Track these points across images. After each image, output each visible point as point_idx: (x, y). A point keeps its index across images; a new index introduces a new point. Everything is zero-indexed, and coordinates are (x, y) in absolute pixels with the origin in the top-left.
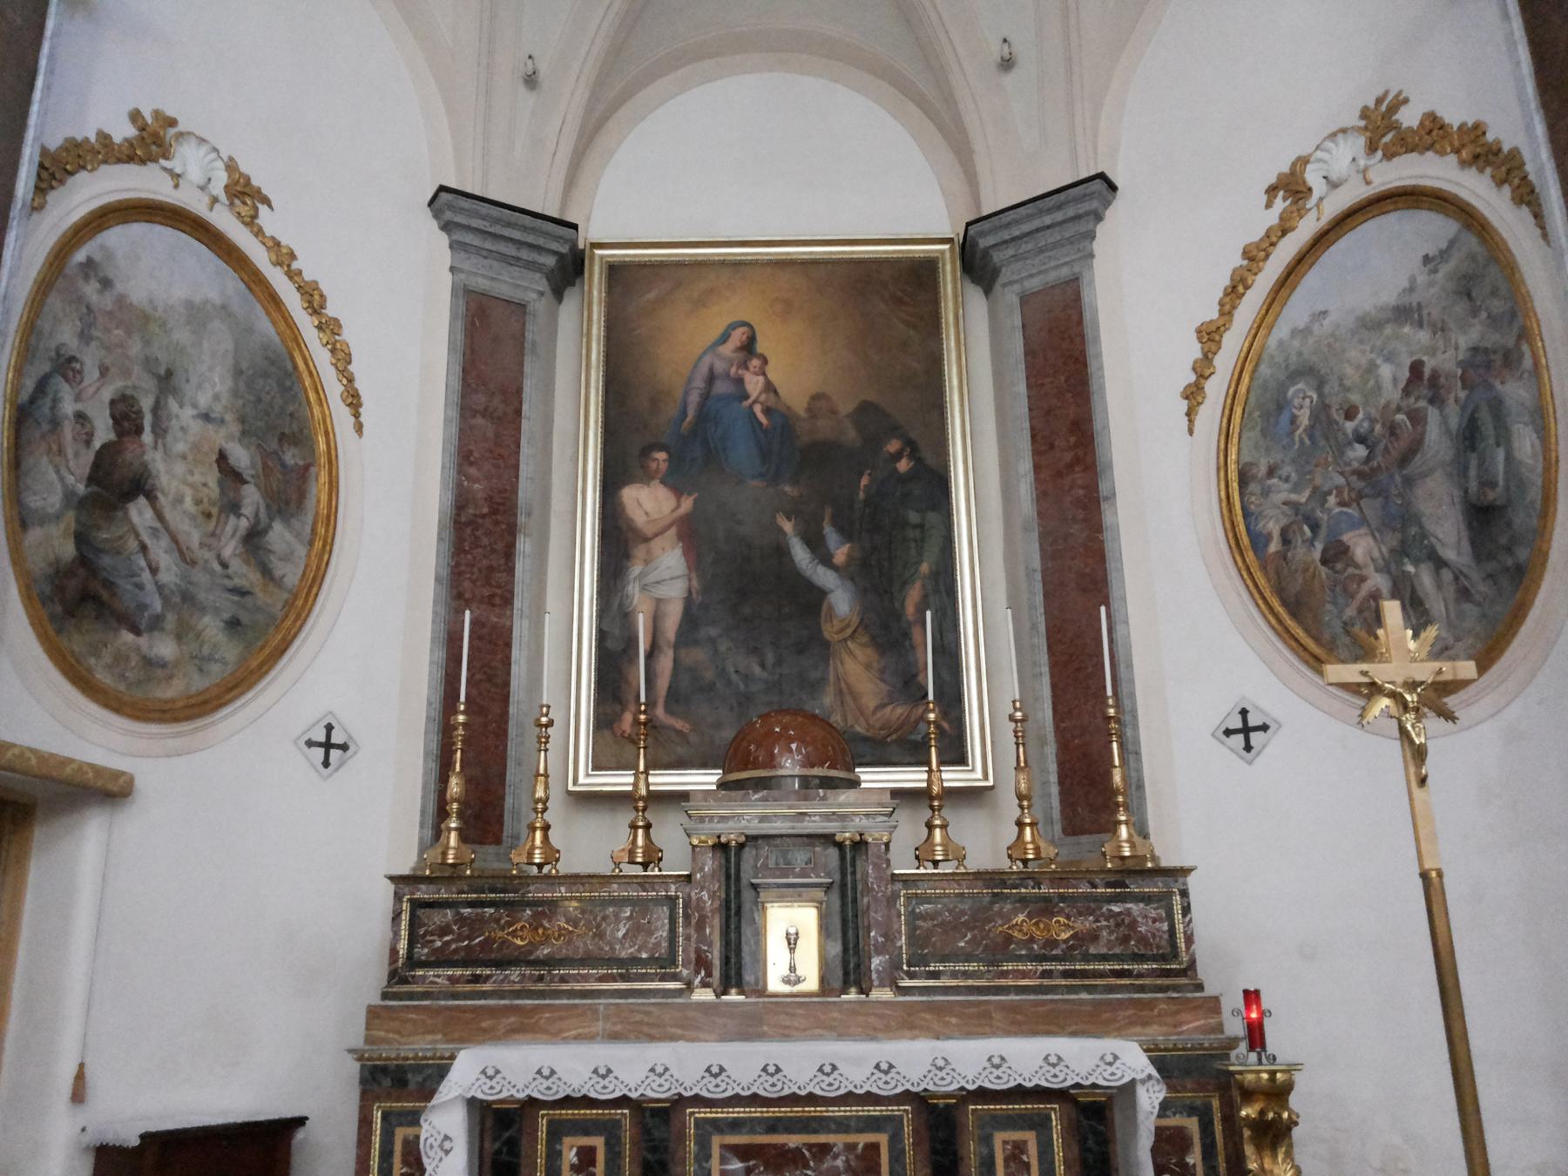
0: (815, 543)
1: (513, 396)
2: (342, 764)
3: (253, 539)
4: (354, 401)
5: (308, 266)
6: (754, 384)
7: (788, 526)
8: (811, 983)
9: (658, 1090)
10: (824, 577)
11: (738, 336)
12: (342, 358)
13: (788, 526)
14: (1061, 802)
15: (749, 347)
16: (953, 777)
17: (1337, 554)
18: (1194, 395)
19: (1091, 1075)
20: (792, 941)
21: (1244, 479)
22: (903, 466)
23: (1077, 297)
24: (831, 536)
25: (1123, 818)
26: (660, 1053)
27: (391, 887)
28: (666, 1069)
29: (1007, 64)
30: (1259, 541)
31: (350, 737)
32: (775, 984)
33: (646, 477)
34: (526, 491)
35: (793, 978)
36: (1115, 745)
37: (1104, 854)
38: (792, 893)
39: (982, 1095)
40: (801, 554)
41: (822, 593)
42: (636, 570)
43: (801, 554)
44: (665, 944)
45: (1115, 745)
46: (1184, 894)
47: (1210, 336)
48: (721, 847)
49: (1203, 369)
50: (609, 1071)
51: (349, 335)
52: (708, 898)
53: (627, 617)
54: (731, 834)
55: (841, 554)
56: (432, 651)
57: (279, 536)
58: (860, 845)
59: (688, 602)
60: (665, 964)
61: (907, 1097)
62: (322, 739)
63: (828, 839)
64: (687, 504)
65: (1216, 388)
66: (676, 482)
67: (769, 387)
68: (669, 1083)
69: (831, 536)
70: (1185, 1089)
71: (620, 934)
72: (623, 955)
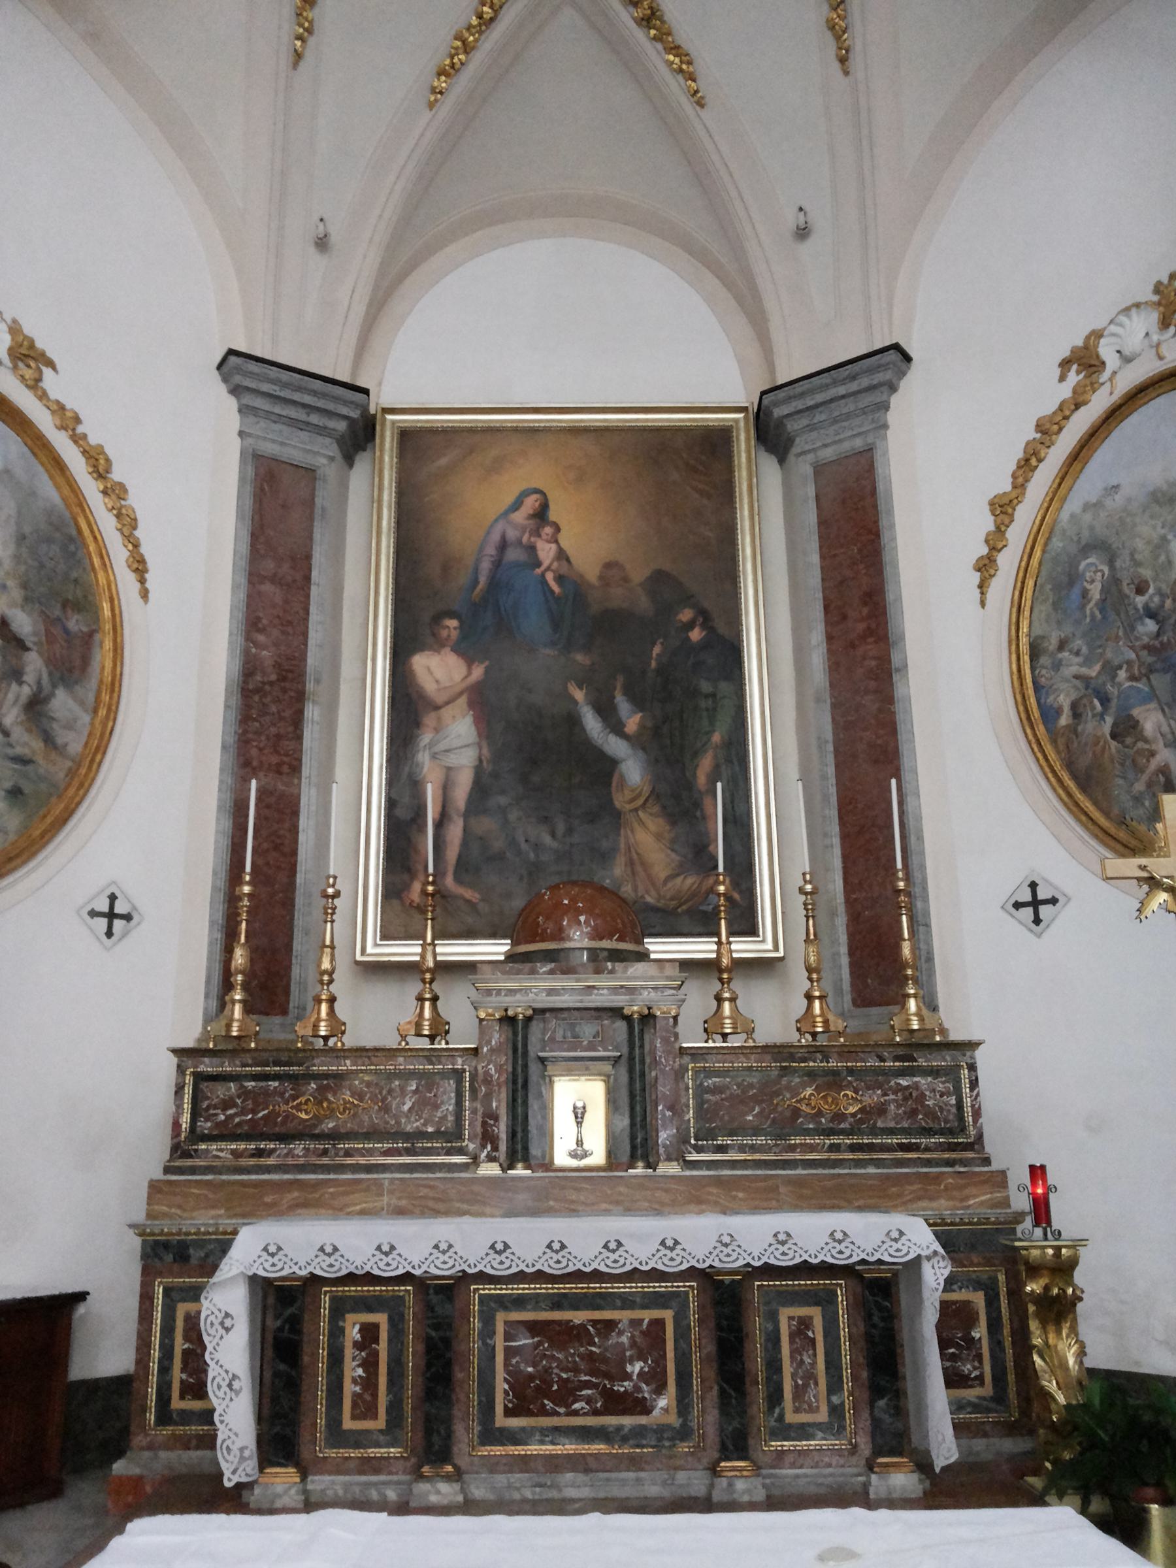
0: (606, 711)
1: (303, 562)
2: (125, 935)
3: (35, 706)
4: (139, 567)
5: (95, 431)
6: (546, 552)
7: (579, 695)
8: (598, 1157)
9: (441, 1267)
10: (615, 746)
11: (531, 503)
12: (128, 523)
13: (579, 695)
14: (852, 973)
15: (541, 515)
16: (743, 948)
17: (1126, 729)
18: (986, 567)
19: (309, 1264)
20: (579, 1115)
21: (1035, 652)
22: (696, 635)
23: (871, 468)
24: (623, 705)
25: (912, 991)
26: (444, 1229)
27: (174, 1060)
28: (393, 1248)
29: (803, 233)
30: (1049, 715)
31: (134, 908)
32: (561, 1158)
33: (437, 644)
34: (314, 659)
35: (579, 1152)
36: (904, 918)
37: (893, 1027)
38: (579, 1066)
39: (768, 1271)
40: (592, 723)
41: (612, 764)
42: (426, 738)
43: (592, 723)
44: (451, 1118)
45: (904, 918)
46: (972, 1067)
47: (1003, 508)
48: (508, 1020)
49: (995, 542)
50: (393, 1248)
51: (134, 500)
52: (495, 1068)
53: (416, 786)
54: (519, 1007)
55: (633, 722)
56: (218, 819)
57: (62, 703)
58: (648, 1018)
59: (478, 770)
60: (451, 1138)
61: (692, 1273)
62: (106, 909)
63: (616, 1012)
64: (478, 672)
65: (1008, 562)
66: (466, 649)
67: (562, 555)
68: (509, 1260)
69: (623, 705)
70: (972, 1265)
71: (406, 1108)
72: (409, 1128)
